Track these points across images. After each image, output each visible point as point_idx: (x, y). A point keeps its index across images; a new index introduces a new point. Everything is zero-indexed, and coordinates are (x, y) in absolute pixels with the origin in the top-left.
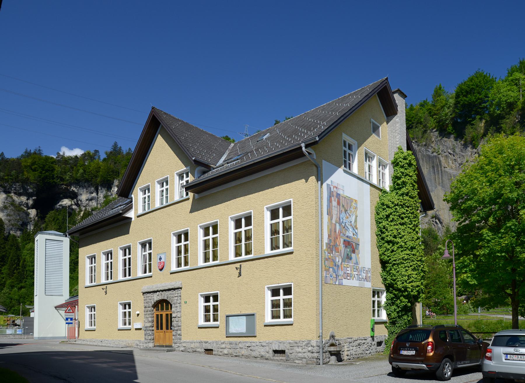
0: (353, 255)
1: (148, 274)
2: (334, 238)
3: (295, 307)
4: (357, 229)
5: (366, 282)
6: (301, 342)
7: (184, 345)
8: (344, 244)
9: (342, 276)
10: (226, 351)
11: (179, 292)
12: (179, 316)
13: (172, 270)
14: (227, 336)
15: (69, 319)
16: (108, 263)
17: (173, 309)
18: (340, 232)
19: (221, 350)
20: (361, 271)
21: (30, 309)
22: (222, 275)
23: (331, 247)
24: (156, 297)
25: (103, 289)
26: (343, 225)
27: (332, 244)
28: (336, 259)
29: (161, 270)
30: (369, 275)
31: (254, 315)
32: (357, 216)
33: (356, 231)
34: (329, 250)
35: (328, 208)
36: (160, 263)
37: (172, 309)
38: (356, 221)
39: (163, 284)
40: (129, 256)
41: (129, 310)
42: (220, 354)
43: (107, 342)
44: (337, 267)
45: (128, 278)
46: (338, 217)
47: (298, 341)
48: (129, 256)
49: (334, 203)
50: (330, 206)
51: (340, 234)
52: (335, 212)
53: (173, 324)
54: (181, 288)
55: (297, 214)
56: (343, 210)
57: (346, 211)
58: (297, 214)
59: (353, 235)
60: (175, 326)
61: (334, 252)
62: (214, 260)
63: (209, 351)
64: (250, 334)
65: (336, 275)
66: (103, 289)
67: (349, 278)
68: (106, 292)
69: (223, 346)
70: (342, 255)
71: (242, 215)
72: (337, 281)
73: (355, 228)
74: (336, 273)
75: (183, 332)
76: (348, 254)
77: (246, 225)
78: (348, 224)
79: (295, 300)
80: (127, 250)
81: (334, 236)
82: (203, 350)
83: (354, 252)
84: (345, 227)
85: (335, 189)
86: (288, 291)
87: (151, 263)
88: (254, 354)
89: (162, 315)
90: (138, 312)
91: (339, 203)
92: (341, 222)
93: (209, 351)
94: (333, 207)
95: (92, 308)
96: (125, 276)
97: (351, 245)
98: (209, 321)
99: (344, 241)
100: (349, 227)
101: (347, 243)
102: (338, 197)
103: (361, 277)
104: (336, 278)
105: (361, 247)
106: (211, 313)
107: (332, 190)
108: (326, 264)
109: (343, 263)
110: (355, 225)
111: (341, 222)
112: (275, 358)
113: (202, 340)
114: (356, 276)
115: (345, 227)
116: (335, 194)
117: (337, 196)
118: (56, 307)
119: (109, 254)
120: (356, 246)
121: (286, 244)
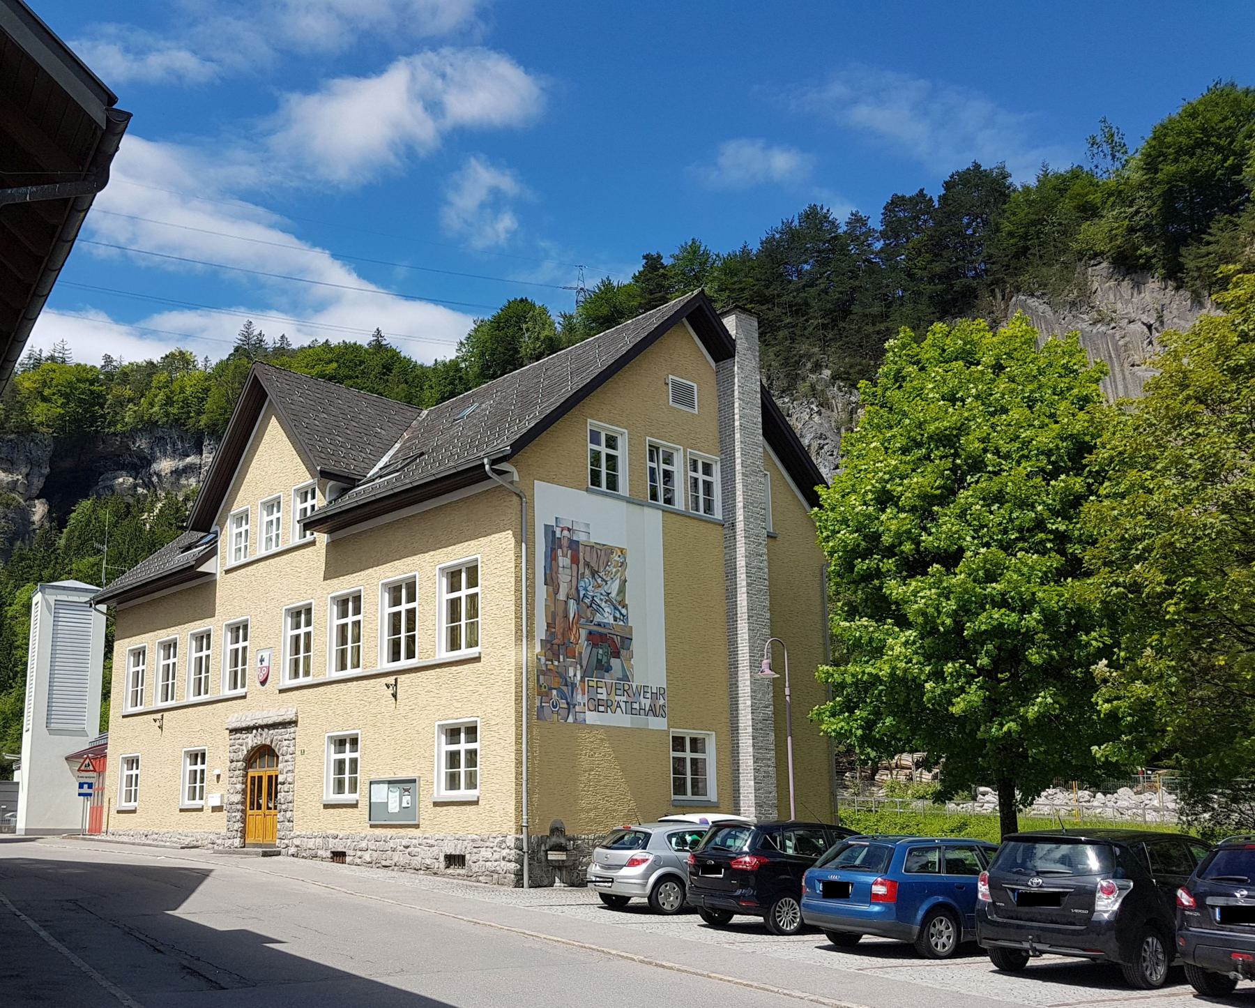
0: (614, 662)
1: (464, 652)
2: (561, 630)
3: (482, 767)
4: (625, 606)
5: (651, 718)
6: (491, 839)
7: (297, 842)
8: (588, 640)
9: (584, 705)
10: (367, 857)
11: (292, 730)
12: (289, 780)
13: (437, 657)
14: (372, 823)
15: (86, 786)
16: (344, 626)
17: (280, 766)
18: (579, 615)
19: (359, 853)
20: (637, 695)
21: (14, 761)
22: (365, 698)
23: (555, 647)
24: (251, 740)
25: (155, 720)
26: (587, 601)
27: (556, 641)
28: (567, 671)
29: (263, 683)
30: (662, 702)
31: (414, 781)
32: (625, 581)
33: (624, 611)
34: (550, 654)
35: (548, 572)
36: (261, 668)
37: (279, 765)
38: (622, 590)
39: (265, 714)
40: (308, 629)
41: (354, 755)
42: (358, 861)
43: (156, 836)
44: (570, 688)
45: (350, 672)
46: (574, 587)
47: (486, 837)
48: (308, 629)
49: (564, 561)
50: (551, 569)
51: (578, 620)
52: (564, 578)
53: (279, 797)
54: (293, 723)
55: (486, 583)
56: (587, 572)
57: (594, 573)
58: (486, 583)
59: (615, 620)
60: (282, 802)
61: (561, 657)
62: (470, 645)
63: (338, 856)
64: (408, 820)
65: (568, 704)
66: (155, 720)
67: (601, 709)
68: (395, 696)
69: (363, 845)
70: (584, 663)
71: (349, 594)
72: (570, 716)
73: (619, 604)
74: (566, 699)
75: (296, 815)
76: (601, 660)
77: (408, 601)
78: (601, 600)
79: (483, 752)
80: (203, 639)
81: (562, 625)
82: (329, 854)
83: (617, 655)
84: (591, 606)
85: (566, 533)
86: (472, 732)
87: (414, 635)
88: (416, 862)
89: (261, 777)
90: (217, 772)
91: (575, 560)
92: (581, 596)
93: (338, 856)
94: (561, 569)
95: (133, 762)
96: (343, 667)
97: (610, 642)
98: (194, 799)
99: (590, 633)
100: (603, 605)
101: (596, 638)
102: (574, 546)
103: (636, 706)
104: (569, 709)
105: (635, 645)
106: (463, 769)
107: (558, 535)
108: (541, 682)
109: (587, 679)
110: (619, 599)
111: (581, 596)
112: (449, 871)
113: (329, 832)
114: (623, 705)
115: (593, 605)
116: (565, 543)
117: (569, 547)
118: (67, 759)
119: (170, 647)
120: (623, 642)
121: (473, 643)
